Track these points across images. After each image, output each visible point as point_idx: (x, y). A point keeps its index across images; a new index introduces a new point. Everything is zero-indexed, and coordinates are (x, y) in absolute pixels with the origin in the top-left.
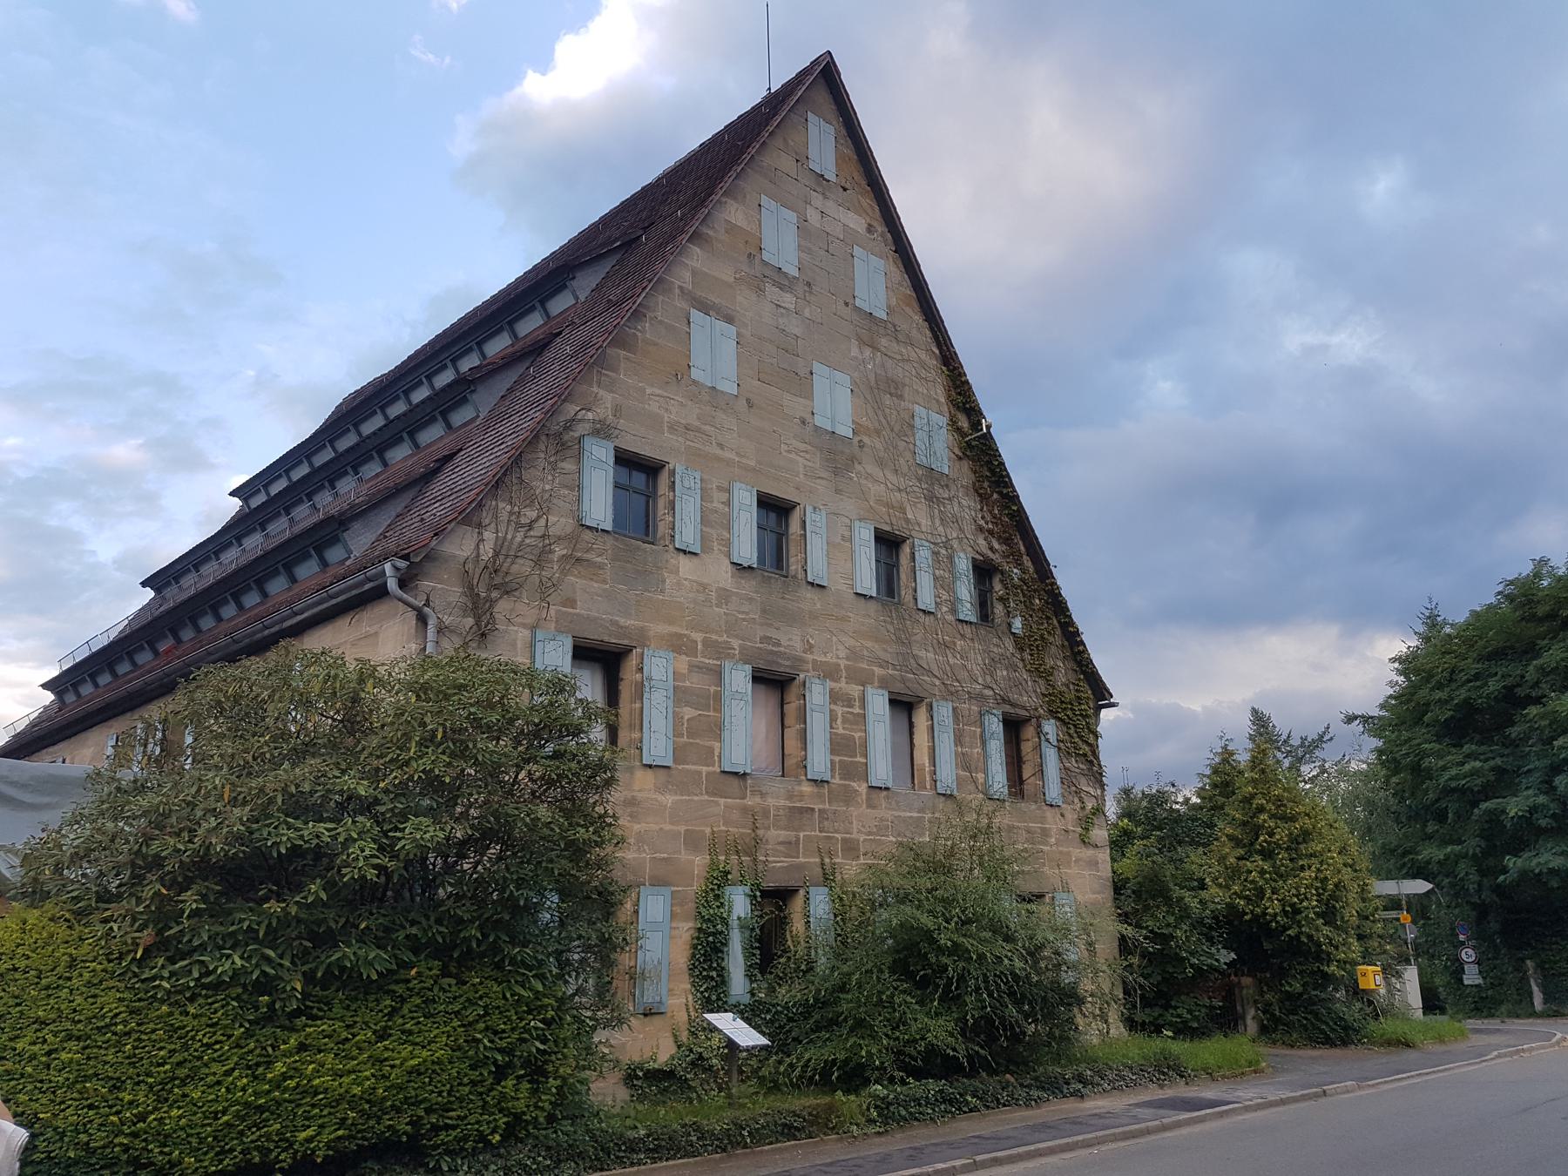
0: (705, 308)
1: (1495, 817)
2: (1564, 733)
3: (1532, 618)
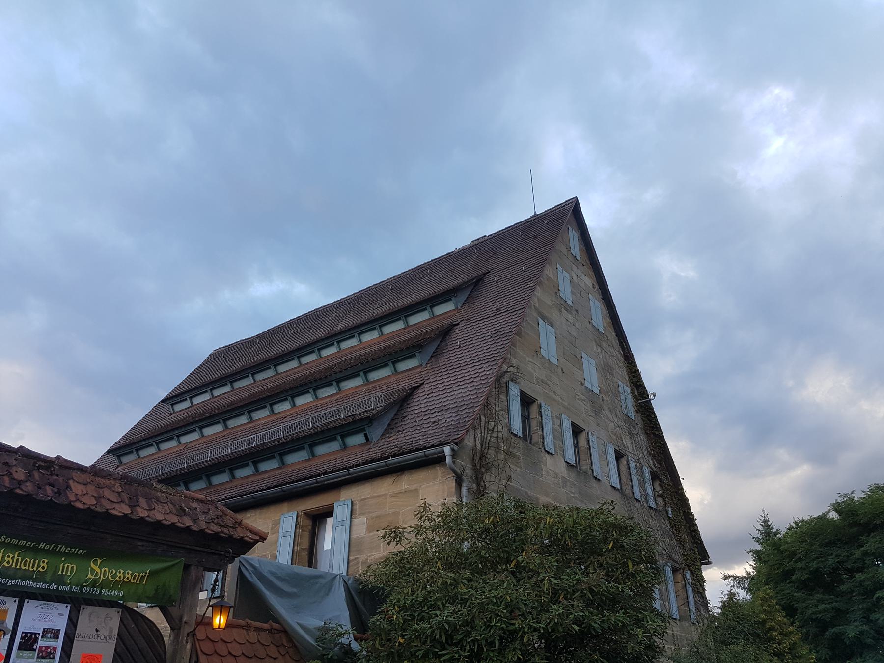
0: (544, 318)
1: (838, 639)
2: (880, 589)
3: (856, 524)
